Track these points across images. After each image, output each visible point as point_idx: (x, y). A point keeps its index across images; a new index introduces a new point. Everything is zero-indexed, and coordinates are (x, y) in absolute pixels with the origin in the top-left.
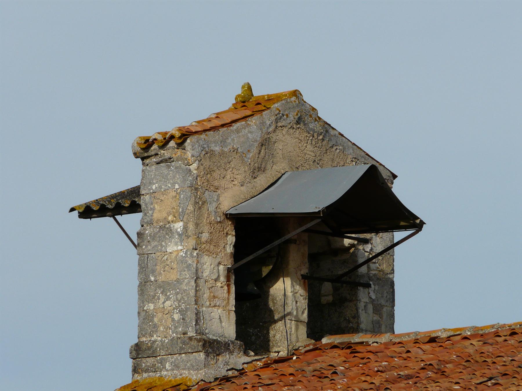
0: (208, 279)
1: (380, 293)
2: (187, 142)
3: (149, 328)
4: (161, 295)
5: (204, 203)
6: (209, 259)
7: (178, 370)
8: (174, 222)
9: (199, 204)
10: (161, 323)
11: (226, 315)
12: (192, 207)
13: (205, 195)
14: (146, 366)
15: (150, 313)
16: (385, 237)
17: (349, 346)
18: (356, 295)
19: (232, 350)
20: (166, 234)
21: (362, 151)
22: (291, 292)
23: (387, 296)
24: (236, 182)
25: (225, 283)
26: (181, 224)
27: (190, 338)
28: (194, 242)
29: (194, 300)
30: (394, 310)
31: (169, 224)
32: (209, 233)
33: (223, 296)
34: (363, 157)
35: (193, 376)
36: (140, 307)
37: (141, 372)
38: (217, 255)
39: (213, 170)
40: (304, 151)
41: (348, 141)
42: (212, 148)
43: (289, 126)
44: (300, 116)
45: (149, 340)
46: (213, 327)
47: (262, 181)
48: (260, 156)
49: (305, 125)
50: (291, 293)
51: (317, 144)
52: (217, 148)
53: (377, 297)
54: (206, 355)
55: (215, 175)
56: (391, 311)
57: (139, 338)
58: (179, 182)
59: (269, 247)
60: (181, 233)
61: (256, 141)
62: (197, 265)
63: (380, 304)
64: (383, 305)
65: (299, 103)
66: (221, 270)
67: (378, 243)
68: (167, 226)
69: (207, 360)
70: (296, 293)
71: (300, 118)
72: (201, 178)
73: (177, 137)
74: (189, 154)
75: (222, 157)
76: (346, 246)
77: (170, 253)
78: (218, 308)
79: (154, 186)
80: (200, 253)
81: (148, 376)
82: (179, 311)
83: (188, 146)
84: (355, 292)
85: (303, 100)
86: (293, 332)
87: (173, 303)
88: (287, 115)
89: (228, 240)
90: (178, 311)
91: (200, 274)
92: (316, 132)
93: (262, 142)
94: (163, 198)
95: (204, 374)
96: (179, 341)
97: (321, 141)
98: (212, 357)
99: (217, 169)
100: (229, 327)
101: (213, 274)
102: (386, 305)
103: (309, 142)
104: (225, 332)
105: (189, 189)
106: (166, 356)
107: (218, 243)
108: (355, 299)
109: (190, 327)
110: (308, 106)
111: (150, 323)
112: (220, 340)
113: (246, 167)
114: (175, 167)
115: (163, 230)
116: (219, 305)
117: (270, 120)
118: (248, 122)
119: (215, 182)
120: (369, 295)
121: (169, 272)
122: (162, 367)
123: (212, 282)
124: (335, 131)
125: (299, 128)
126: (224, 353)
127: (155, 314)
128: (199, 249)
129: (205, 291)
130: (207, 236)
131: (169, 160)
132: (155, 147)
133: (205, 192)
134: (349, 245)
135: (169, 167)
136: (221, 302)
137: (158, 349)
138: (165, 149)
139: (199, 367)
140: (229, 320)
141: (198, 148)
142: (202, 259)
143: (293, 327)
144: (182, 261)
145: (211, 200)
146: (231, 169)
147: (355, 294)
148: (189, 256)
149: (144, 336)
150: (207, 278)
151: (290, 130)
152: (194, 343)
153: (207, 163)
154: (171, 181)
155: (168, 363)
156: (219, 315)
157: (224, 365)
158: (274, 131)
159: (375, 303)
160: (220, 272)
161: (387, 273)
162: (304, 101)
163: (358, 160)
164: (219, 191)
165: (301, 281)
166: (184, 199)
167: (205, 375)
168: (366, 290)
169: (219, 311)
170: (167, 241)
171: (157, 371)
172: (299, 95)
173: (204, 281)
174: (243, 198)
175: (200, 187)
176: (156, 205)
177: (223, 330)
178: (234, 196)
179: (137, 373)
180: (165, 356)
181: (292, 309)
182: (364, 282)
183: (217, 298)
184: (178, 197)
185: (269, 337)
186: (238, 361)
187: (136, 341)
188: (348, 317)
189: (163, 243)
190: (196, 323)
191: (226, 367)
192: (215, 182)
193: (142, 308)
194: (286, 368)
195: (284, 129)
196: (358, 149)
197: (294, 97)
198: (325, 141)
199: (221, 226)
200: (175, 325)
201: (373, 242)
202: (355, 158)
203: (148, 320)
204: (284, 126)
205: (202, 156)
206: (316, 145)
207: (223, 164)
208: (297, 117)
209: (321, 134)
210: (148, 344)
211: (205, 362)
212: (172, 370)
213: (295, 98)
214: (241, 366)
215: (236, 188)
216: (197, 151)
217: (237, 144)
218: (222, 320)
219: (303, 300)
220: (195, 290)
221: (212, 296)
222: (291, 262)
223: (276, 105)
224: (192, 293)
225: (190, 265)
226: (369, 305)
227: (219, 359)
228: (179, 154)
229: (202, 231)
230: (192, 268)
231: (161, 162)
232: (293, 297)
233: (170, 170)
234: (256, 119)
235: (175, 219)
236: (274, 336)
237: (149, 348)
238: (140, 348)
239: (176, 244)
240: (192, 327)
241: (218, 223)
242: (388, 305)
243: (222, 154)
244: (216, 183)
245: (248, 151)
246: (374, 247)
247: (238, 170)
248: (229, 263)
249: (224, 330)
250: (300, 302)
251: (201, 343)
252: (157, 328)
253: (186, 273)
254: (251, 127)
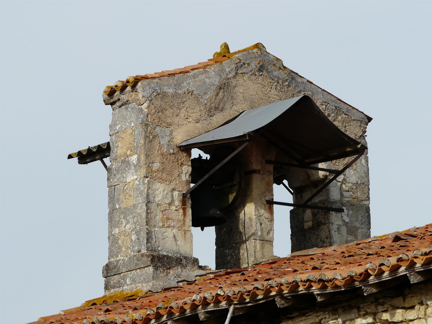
0: (161, 203)
1: (355, 217)
2: (138, 85)
3: (116, 250)
4: (123, 220)
5: (154, 137)
6: (161, 186)
7: (135, 284)
8: (131, 156)
9: (149, 138)
10: (124, 245)
11: (182, 234)
12: (143, 141)
13: (156, 130)
14: (113, 283)
15: (116, 237)
16: (359, 169)
18: (328, 218)
19: (185, 264)
20: (126, 166)
21: (333, 97)
22: (255, 215)
23: (361, 220)
24: (191, 120)
25: (181, 206)
26: (136, 156)
27: (142, 255)
28: (145, 170)
29: (145, 221)
30: (370, 232)
31: (128, 158)
32: (161, 163)
33: (178, 218)
34: (334, 101)
35: (144, 288)
36: (109, 232)
37: (110, 289)
38: (170, 182)
39: (165, 109)
40: (268, 95)
41: (317, 87)
42: (165, 90)
43: (251, 73)
44: (262, 65)
45: (116, 260)
46: (166, 245)
47: (219, 118)
48: (217, 98)
49: (268, 72)
50: (255, 216)
51: (283, 89)
52: (170, 90)
53: (351, 220)
54: (155, 269)
55: (169, 112)
56: (367, 233)
57: (109, 259)
58: (134, 121)
59: (212, 172)
60: (136, 164)
61: (214, 85)
62: (148, 190)
63: (354, 226)
64: (357, 227)
65: (261, 54)
66: (176, 196)
67: (351, 174)
68: (127, 160)
69: (156, 273)
70: (261, 216)
71: (261, 67)
72: (152, 115)
73: (131, 81)
74: (140, 95)
75: (175, 98)
76: (320, 178)
77: (129, 183)
78: (173, 228)
79: (118, 126)
80: (152, 180)
81: (114, 291)
82: (136, 232)
83: (139, 88)
84: (328, 216)
85: (266, 51)
86: (258, 250)
87: (131, 226)
88: (249, 64)
89: (183, 170)
90: (134, 233)
91: (151, 199)
92: (281, 79)
93: (220, 86)
94: (123, 136)
95: (152, 285)
96: (135, 258)
97: (287, 87)
98: (162, 271)
99: (170, 108)
100: (184, 245)
101: (166, 199)
102: (361, 227)
103: (274, 87)
104: (180, 250)
105: (141, 125)
106: (127, 272)
107: (172, 171)
108: (327, 222)
109: (143, 245)
110: (272, 57)
111: (116, 245)
112: (171, 255)
113: (202, 106)
114: (131, 108)
115: (124, 164)
116: (173, 226)
117: (230, 67)
118: (207, 69)
119: (168, 119)
120: (342, 219)
121: (128, 199)
122: (124, 282)
123: (165, 206)
124: (303, 79)
125: (261, 75)
126: (176, 267)
127: (119, 237)
128: (150, 177)
129: (157, 214)
130: (159, 166)
131: (126, 103)
132: (118, 93)
133: (155, 128)
134: (324, 177)
135: (127, 108)
136: (175, 223)
137: (121, 267)
138: (124, 93)
139: (149, 280)
140: (185, 239)
141: (149, 90)
142: (154, 185)
143: (258, 246)
144: (138, 189)
145: (163, 134)
146: (185, 109)
147: (327, 218)
148: (141, 184)
149: (112, 257)
150: (160, 202)
151: (251, 76)
152: (145, 259)
153: (158, 103)
154: (129, 121)
155: (128, 278)
156: (173, 234)
157: (175, 277)
158: (234, 77)
159: (348, 225)
160: (174, 197)
161: (362, 200)
162: (267, 52)
163: (329, 104)
164: (172, 127)
165: (266, 205)
166: (137, 134)
167: (153, 286)
168: (339, 215)
169: (174, 231)
170: (127, 173)
171: (121, 287)
172: (262, 48)
173: (156, 204)
174: (197, 133)
175: (150, 123)
176: (119, 143)
177: (178, 247)
178: (188, 131)
179: (107, 290)
180: (126, 273)
181: (256, 230)
182: (337, 207)
183: (171, 219)
184: (133, 134)
185: (240, 256)
186: (191, 274)
187: (107, 262)
188: (323, 238)
189: (124, 175)
190: (147, 241)
191: (177, 279)
192: (168, 119)
193: (110, 233)
195: (245, 75)
196: (328, 95)
197: (256, 49)
198: (291, 87)
199: (175, 157)
200: (133, 244)
201: (347, 173)
202: (325, 102)
203: (115, 243)
204: (245, 73)
205: (153, 96)
206: (281, 90)
207: (176, 104)
208: (258, 66)
209: (286, 81)
210: (114, 263)
211: (153, 275)
212: (131, 284)
213: (257, 49)
214: (193, 278)
215: (191, 124)
216: (148, 92)
217: (193, 87)
218: (177, 239)
219: (268, 222)
220: (146, 213)
221: (165, 218)
222: (254, 189)
223: (237, 56)
224: (144, 215)
225: (142, 191)
226: (342, 227)
227: (169, 273)
228: (134, 96)
229: (153, 161)
230: (144, 194)
231: (122, 105)
232: (257, 219)
233: (128, 111)
234: (215, 67)
235: (131, 152)
236: (243, 255)
237: (115, 267)
238: (109, 267)
239: (133, 175)
240: (144, 245)
241: (170, 154)
242: (364, 227)
243: (175, 95)
244: (169, 120)
245: (205, 93)
246: (347, 177)
247: (193, 109)
249: (179, 247)
250: (265, 224)
251: (149, 259)
252: (121, 249)
253: (139, 198)
254: (210, 74)
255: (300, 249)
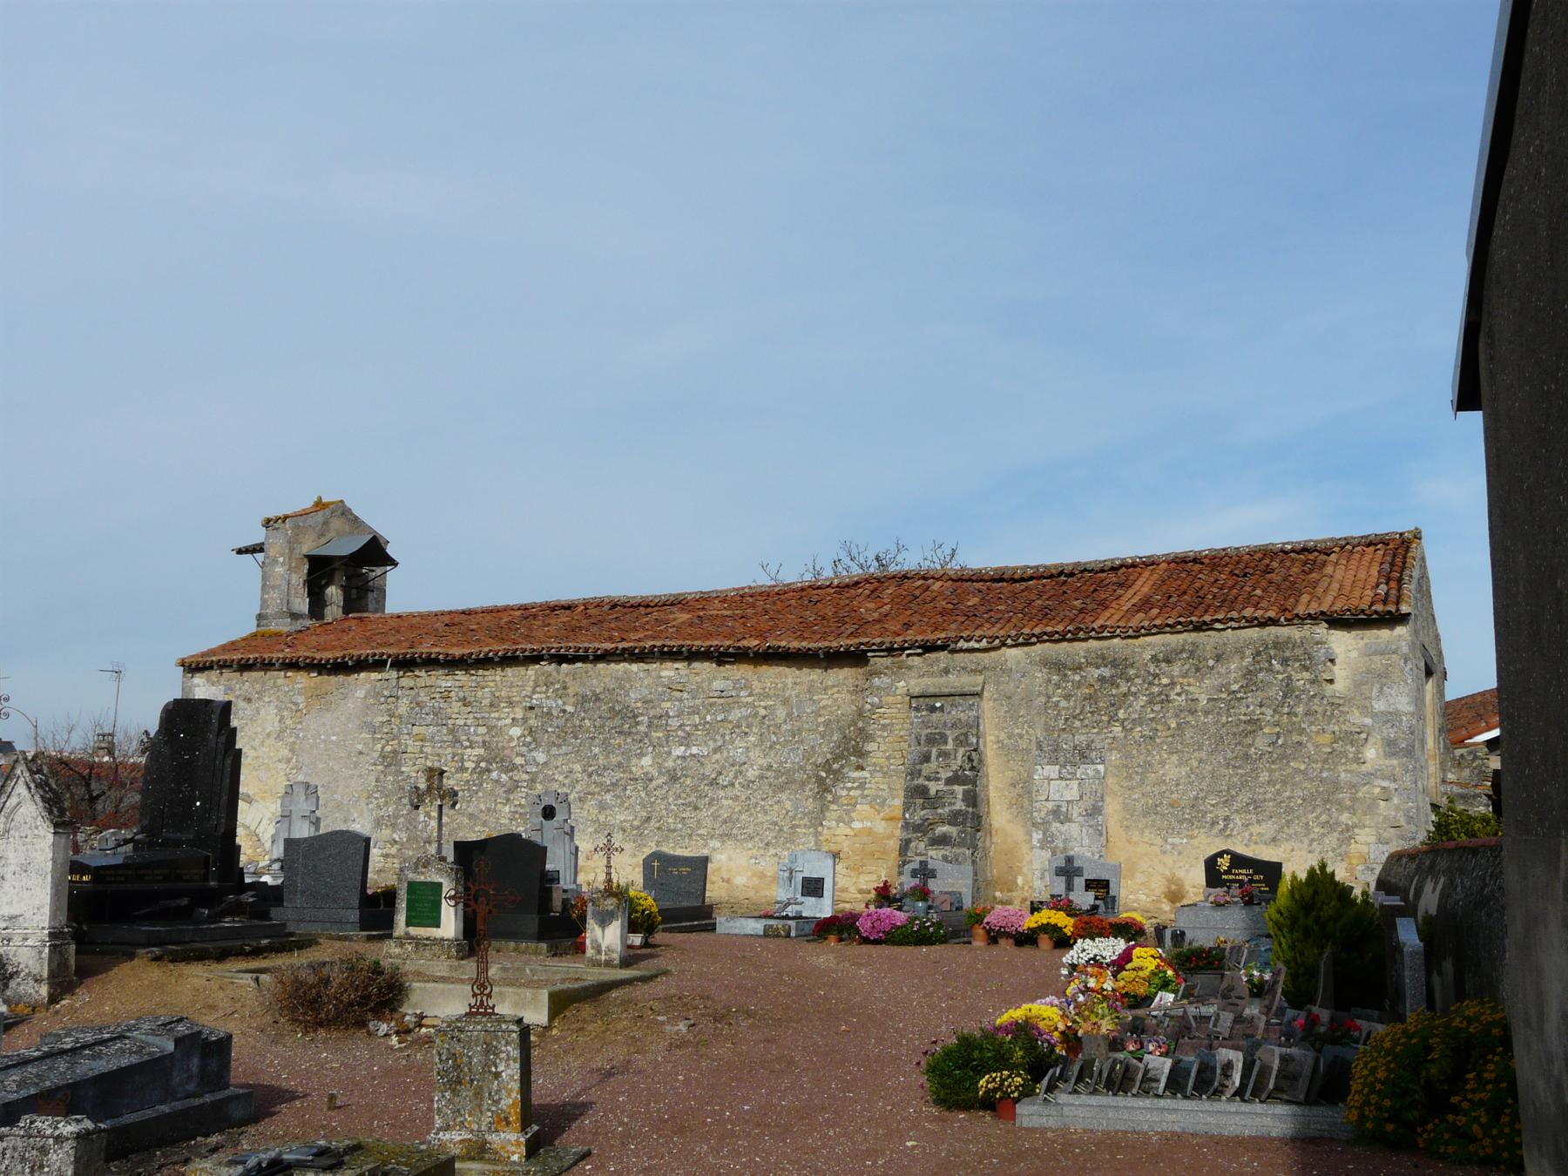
17: (361, 619)
47: (323, 540)
194: (329, 627)
243: (304, 527)
248: (305, 578)
255: (1399, 995)
